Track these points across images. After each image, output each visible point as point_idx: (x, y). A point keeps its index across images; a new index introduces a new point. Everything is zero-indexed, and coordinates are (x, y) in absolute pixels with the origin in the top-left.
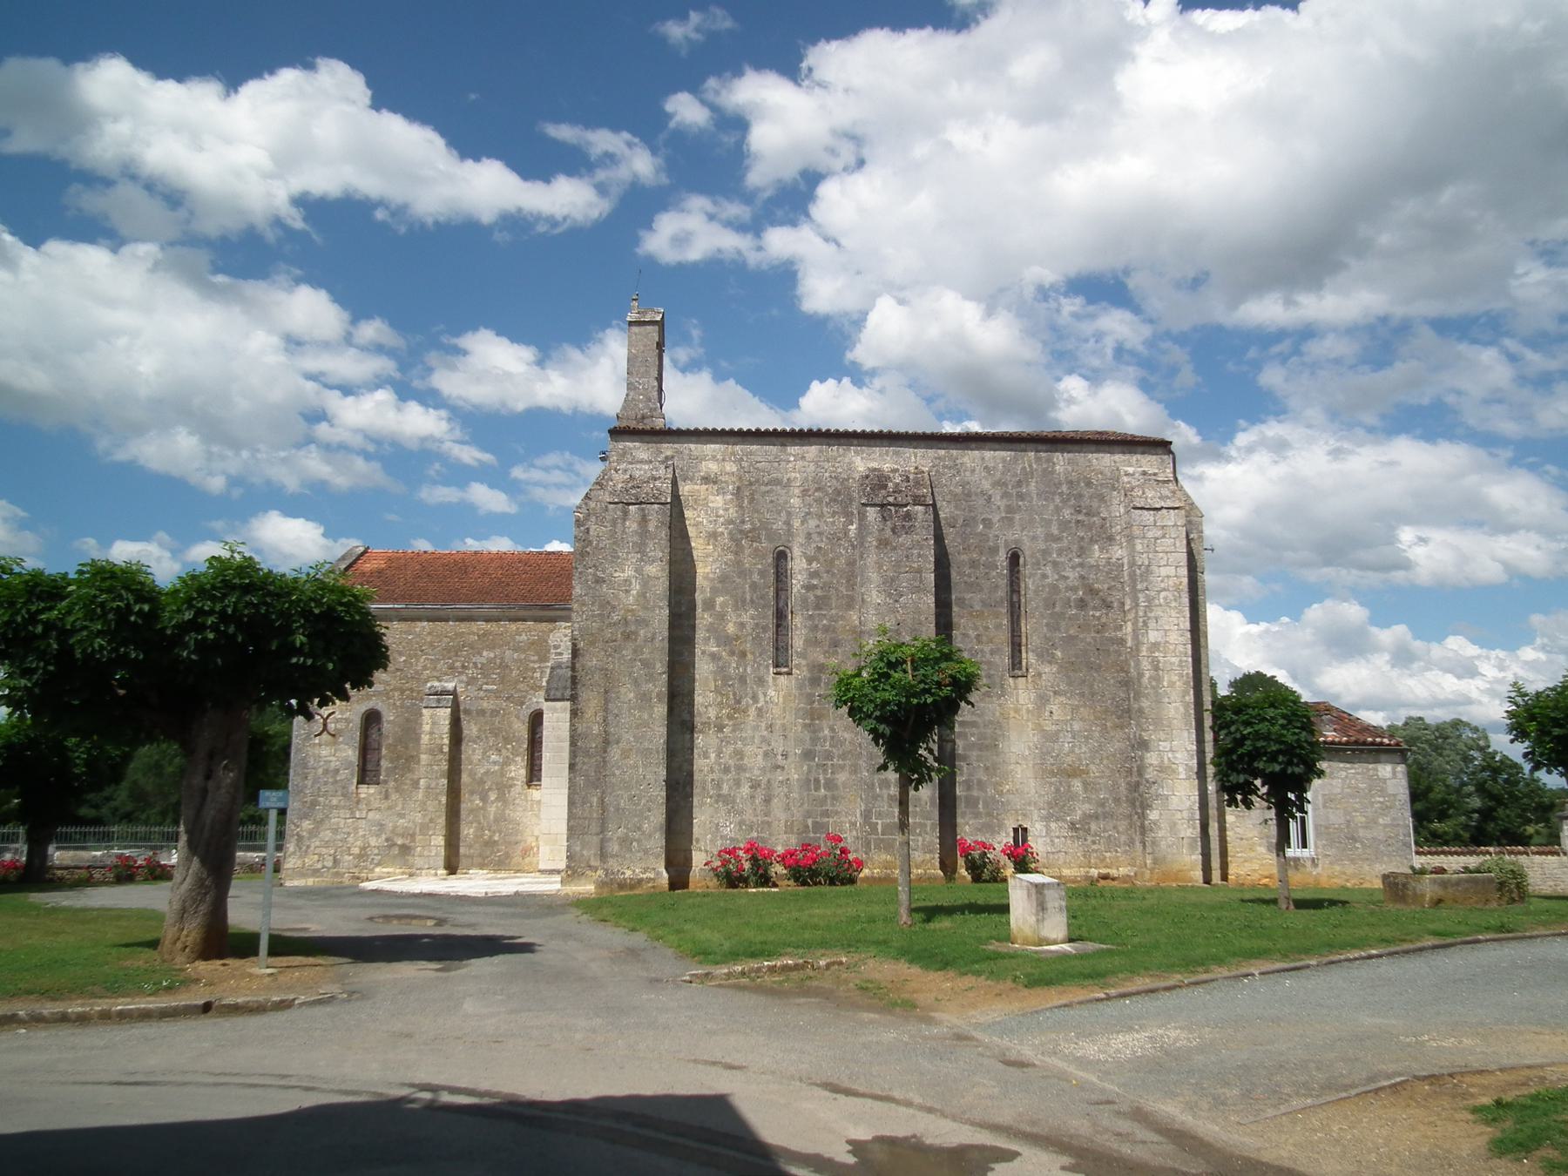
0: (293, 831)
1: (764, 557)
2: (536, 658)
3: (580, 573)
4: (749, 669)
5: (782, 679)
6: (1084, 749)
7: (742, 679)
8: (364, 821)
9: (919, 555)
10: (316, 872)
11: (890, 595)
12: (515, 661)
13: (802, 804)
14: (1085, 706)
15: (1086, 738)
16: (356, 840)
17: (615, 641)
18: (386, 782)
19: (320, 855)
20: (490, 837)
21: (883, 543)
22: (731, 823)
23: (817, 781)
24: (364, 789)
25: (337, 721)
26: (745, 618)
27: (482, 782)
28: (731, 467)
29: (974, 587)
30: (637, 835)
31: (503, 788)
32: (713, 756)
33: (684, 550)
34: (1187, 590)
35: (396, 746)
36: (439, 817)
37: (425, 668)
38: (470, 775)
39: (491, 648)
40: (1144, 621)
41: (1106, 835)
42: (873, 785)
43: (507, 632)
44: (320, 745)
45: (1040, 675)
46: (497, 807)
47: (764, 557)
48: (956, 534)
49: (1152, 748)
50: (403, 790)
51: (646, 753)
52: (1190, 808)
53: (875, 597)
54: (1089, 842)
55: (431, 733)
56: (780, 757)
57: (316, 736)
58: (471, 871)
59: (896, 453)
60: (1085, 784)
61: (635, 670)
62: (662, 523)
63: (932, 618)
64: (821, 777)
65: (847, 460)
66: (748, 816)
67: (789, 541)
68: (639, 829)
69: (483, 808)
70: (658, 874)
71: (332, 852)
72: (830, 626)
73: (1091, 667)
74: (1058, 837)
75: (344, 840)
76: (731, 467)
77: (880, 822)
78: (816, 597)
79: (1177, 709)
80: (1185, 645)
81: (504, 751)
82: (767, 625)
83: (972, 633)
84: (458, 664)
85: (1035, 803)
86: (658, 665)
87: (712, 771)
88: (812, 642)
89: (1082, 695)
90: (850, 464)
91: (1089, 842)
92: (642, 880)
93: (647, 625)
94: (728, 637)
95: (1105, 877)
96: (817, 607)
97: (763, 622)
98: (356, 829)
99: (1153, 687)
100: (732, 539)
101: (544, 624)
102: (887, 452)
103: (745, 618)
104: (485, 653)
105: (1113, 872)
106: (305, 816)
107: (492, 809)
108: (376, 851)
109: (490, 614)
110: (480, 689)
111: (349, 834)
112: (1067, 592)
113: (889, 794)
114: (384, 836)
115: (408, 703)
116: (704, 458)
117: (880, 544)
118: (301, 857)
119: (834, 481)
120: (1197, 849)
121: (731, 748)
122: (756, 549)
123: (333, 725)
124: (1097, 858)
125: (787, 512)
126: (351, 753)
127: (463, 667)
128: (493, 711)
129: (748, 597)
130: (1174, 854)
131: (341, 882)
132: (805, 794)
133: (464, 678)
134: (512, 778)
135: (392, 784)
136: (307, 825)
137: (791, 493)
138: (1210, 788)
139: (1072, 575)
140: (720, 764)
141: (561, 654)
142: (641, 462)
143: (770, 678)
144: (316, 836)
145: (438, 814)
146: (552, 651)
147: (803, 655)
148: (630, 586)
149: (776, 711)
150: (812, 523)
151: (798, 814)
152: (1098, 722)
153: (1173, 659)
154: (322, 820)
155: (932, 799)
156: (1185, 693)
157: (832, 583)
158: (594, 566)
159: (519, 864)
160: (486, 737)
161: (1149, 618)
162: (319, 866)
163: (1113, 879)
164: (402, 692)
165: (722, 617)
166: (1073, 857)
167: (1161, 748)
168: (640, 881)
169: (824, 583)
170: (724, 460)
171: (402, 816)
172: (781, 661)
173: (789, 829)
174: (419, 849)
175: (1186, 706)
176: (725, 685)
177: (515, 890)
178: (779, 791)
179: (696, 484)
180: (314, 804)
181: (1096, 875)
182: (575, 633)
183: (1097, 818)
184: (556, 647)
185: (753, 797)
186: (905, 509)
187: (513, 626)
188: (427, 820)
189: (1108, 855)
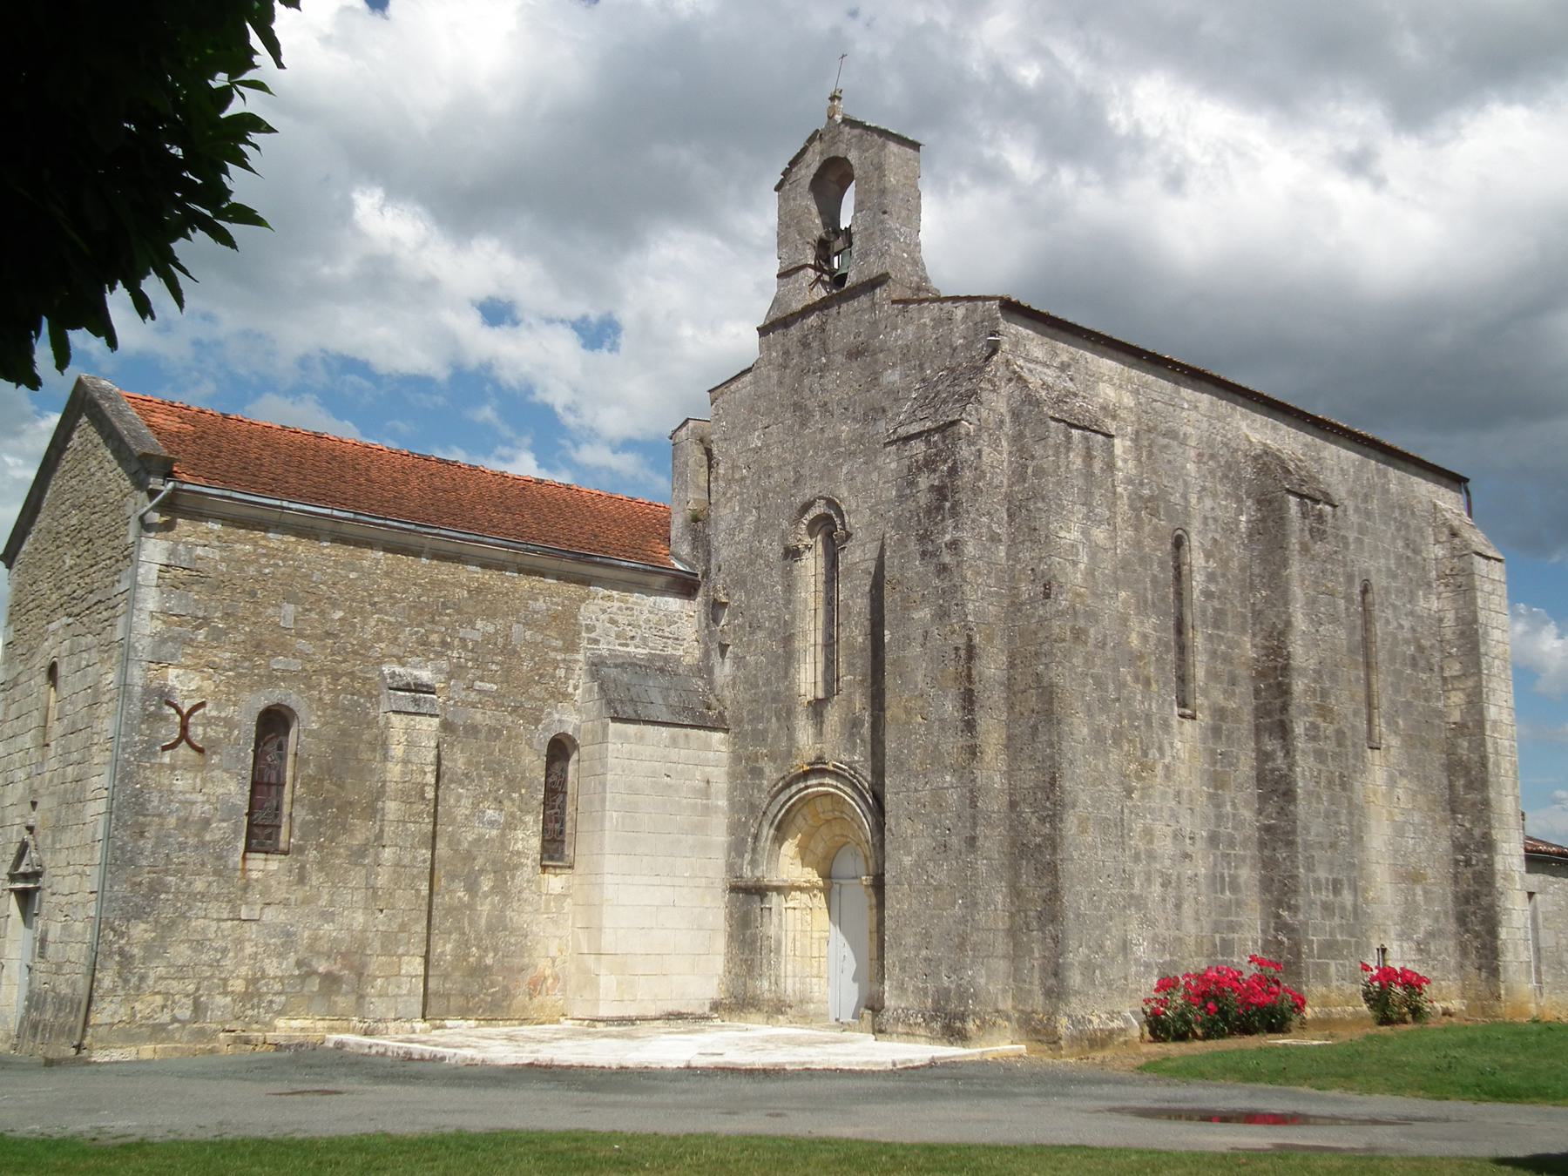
2: (559, 643)
4: (1154, 705)
7: (1148, 718)
8: (254, 927)
10: (157, 1031)
12: (528, 644)
16: (239, 964)
17: (1064, 640)
18: (301, 850)
19: (167, 994)
20: (481, 958)
24: (257, 862)
25: (209, 722)
27: (469, 857)
31: (504, 869)
35: (321, 781)
36: (417, 921)
37: (378, 637)
38: (450, 844)
39: (491, 615)
43: (516, 591)
44: (173, 768)
46: (492, 904)
50: (332, 866)
55: (406, 762)
56: (1188, 841)
57: (165, 749)
58: (448, 1023)
64: (1226, 871)
66: (1161, 930)
67: (1187, 524)
68: (1101, 947)
69: (471, 907)
71: (191, 988)
75: (215, 965)
76: (1128, 400)
81: (507, 803)
84: (435, 638)
88: (1213, 675)
92: (1112, 1032)
94: (1132, 653)
98: (239, 942)
100: (1131, 506)
101: (572, 587)
104: (479, 624)
107: (484, 908)
108: (278, 987)
109: (496, 555)
110: (470, 688)
111: (225, 951)
114: (292, 958)
115: (345, 699)
118: (127, 998)
123: (200, 730)
125: (1184, 480)
126: (236, 791)
127: (444, 643)
128: (491, 729)
131: (212, 1051)
133: (444, 665)
134: (518, 853)
135: (312, 854)
139: (1406, 624)
141: (596, 641)
143: (1175, 721)
144: (158, 956)
145: (414, 914)
146: (584, 634)
150: (1208, 503)
154: (173, 922)
157: (1226, 592)
158: (989, 513)
159: (525, 1008)
160: (480, 777)
162: (165, 1017)
164: (336, 677)
171: (327, 916)
174: (379, 981)
177: (930, 1056)
178: (1189, 891)
180: (156, 888)
184: (590, 629)
187: (525, 583)
188: (395, 927)
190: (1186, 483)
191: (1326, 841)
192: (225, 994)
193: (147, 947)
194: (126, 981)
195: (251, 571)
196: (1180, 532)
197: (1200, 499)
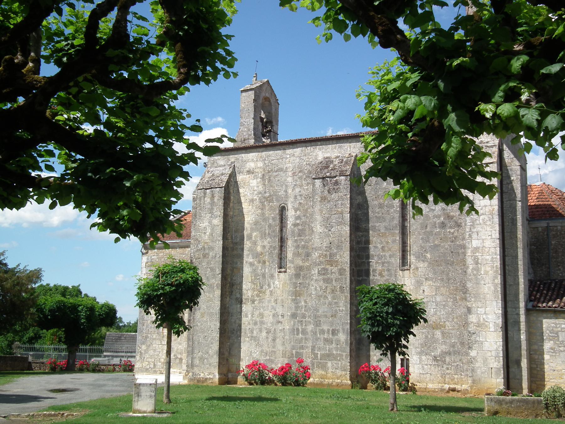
0: (139, 350)
1: (274, 210)
3: (194, 225)
4: (267, 270)
5: (282, 275)
6: (442, 313)
7: (264, 276)
9: (342, 204)
11: (326, 227)
13: (291, 342)
14: (444, 287)
15: (444, 306)
17: (200, 258)
19: (148, 362)
21: (323, 199)
22: (257, 351)
23: (298, 329)
26: (266, 243)
28: (260, 164)
29: (380, 219)
30: (206, 356)
32: (250, 316)
33: (239, 209)
34: (497, 213)
40: (469, 235)
41: (455, 364)
42: (316, 332)
45: (417, 268)
47: (274, 210)
48: (371, 190)
49: (473, 312)
51: (211, 315)
52: (497, 350)
53: (318, 228)
54: (444, 368)
56: (280, 317)
59: (340, 147)
60: (443, 333)
61: (207, 272)
62: (220, 197)
63: (348, 239)
64: (300, 328)
65: (315, 154)
66: (265, 348)
68: (207, 353)
70: (215, 376)
71: (153, 360)
72: (305, 245)
73: (447, 263)
74: (427, 365)
75: (158, 355)
76: (260, 164)
77: (319, 353)
78: (299, 230)
79: (489, 288)
80: (495, 248)
82: (276, 246)
83: (380, 246)
85: (413, 344)
86: (217, 270)
87: (249, 324)
88: (297, 254)
89: (442, 280)
90: (316, 156)
91: (444, 368)
93: (213, 250)
95: (454, 390)
96: (299, 235)
97: (274, 245)
99: (474, 275)
102: (335, 147)
103: (266, 243)
105: (458, 387)
106: (143, 343)
111: (160, 352)
112: (434, 218)
113: (324, 338)
116: (248, 161)
117: (322, 199)
118: (141, 362)
119: (308, 166)
120: (500, 375)
121: (258, 312)
122: (271, 206)
124: (450, 378)
129: (267, 232)
130: (485, 378)
132: (292, 337)
136: (144, 347)
137: (287, 175)
138: (522, 337)
140: (253, 321)
142: (220, 166)
144: (147, 353)
147: (292, 262)
148: (206, 230)
149: (279, 292)
150: (297, 190)
151: (289, 348)
152: (451, 296)
153: (488, 257)
154: (150, 345)
155: (346, 340)
156: (495, 277)
161: (473, 233)
163: (458, 391)
165: (255, 243)
166: (435, 377)
167: (479, 312)
168: (206, 379)
169: (303, 222)
170: (257, 161)
172: (281, 266)
173: (284, 355)
175: (495, 285)
176: (256, 279)
178: (279, 334)
179: (244, 175)
180: (147, 337)
181: (447, 389)
182: (192, 255)
183: (450, 354)
185: (267, 338)
186: (335, 179)
189: (456, 376)
190: (287, 186)
191: (329, 314)
192: (160, 362)
193: (145, 351)
194: (141, 358)
195: (163, 260)
196: (283, 205)
197: (293, 189)
